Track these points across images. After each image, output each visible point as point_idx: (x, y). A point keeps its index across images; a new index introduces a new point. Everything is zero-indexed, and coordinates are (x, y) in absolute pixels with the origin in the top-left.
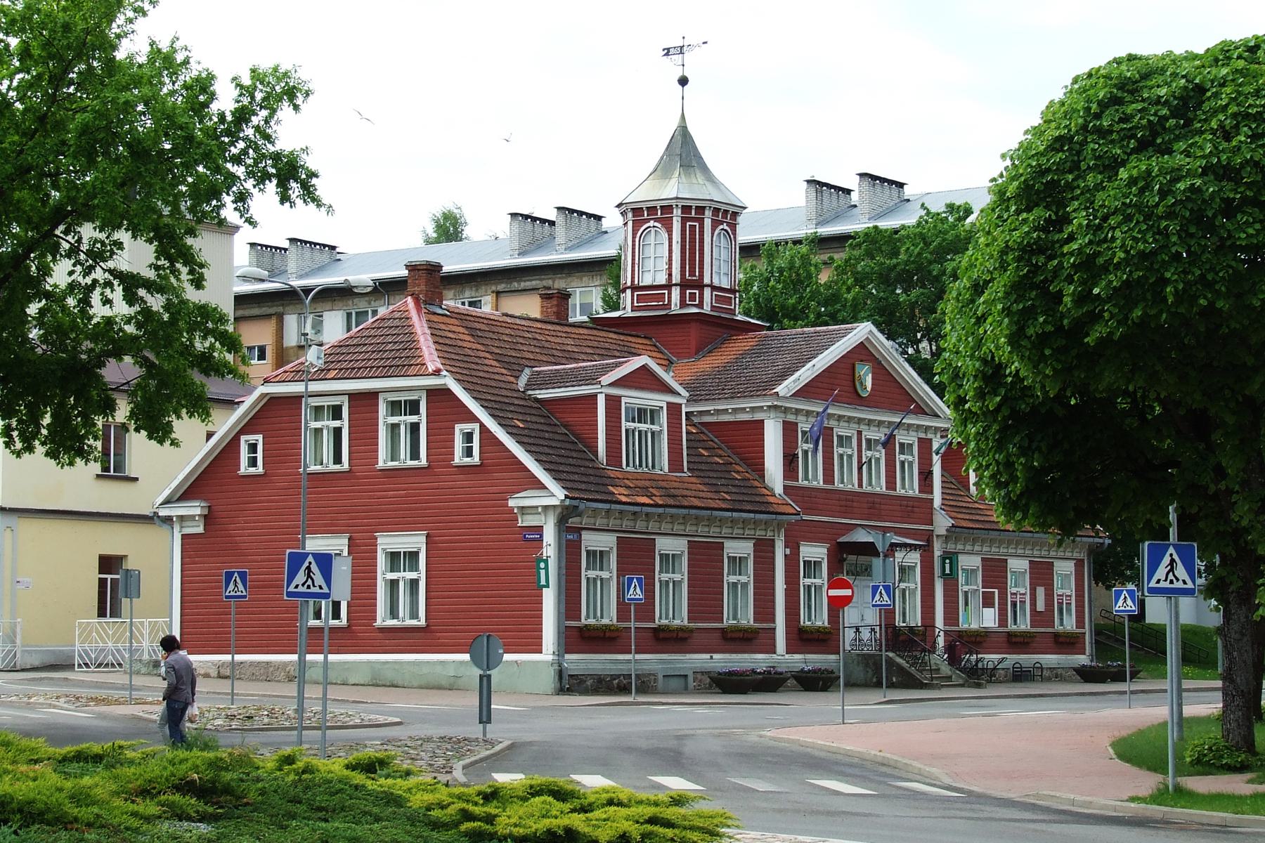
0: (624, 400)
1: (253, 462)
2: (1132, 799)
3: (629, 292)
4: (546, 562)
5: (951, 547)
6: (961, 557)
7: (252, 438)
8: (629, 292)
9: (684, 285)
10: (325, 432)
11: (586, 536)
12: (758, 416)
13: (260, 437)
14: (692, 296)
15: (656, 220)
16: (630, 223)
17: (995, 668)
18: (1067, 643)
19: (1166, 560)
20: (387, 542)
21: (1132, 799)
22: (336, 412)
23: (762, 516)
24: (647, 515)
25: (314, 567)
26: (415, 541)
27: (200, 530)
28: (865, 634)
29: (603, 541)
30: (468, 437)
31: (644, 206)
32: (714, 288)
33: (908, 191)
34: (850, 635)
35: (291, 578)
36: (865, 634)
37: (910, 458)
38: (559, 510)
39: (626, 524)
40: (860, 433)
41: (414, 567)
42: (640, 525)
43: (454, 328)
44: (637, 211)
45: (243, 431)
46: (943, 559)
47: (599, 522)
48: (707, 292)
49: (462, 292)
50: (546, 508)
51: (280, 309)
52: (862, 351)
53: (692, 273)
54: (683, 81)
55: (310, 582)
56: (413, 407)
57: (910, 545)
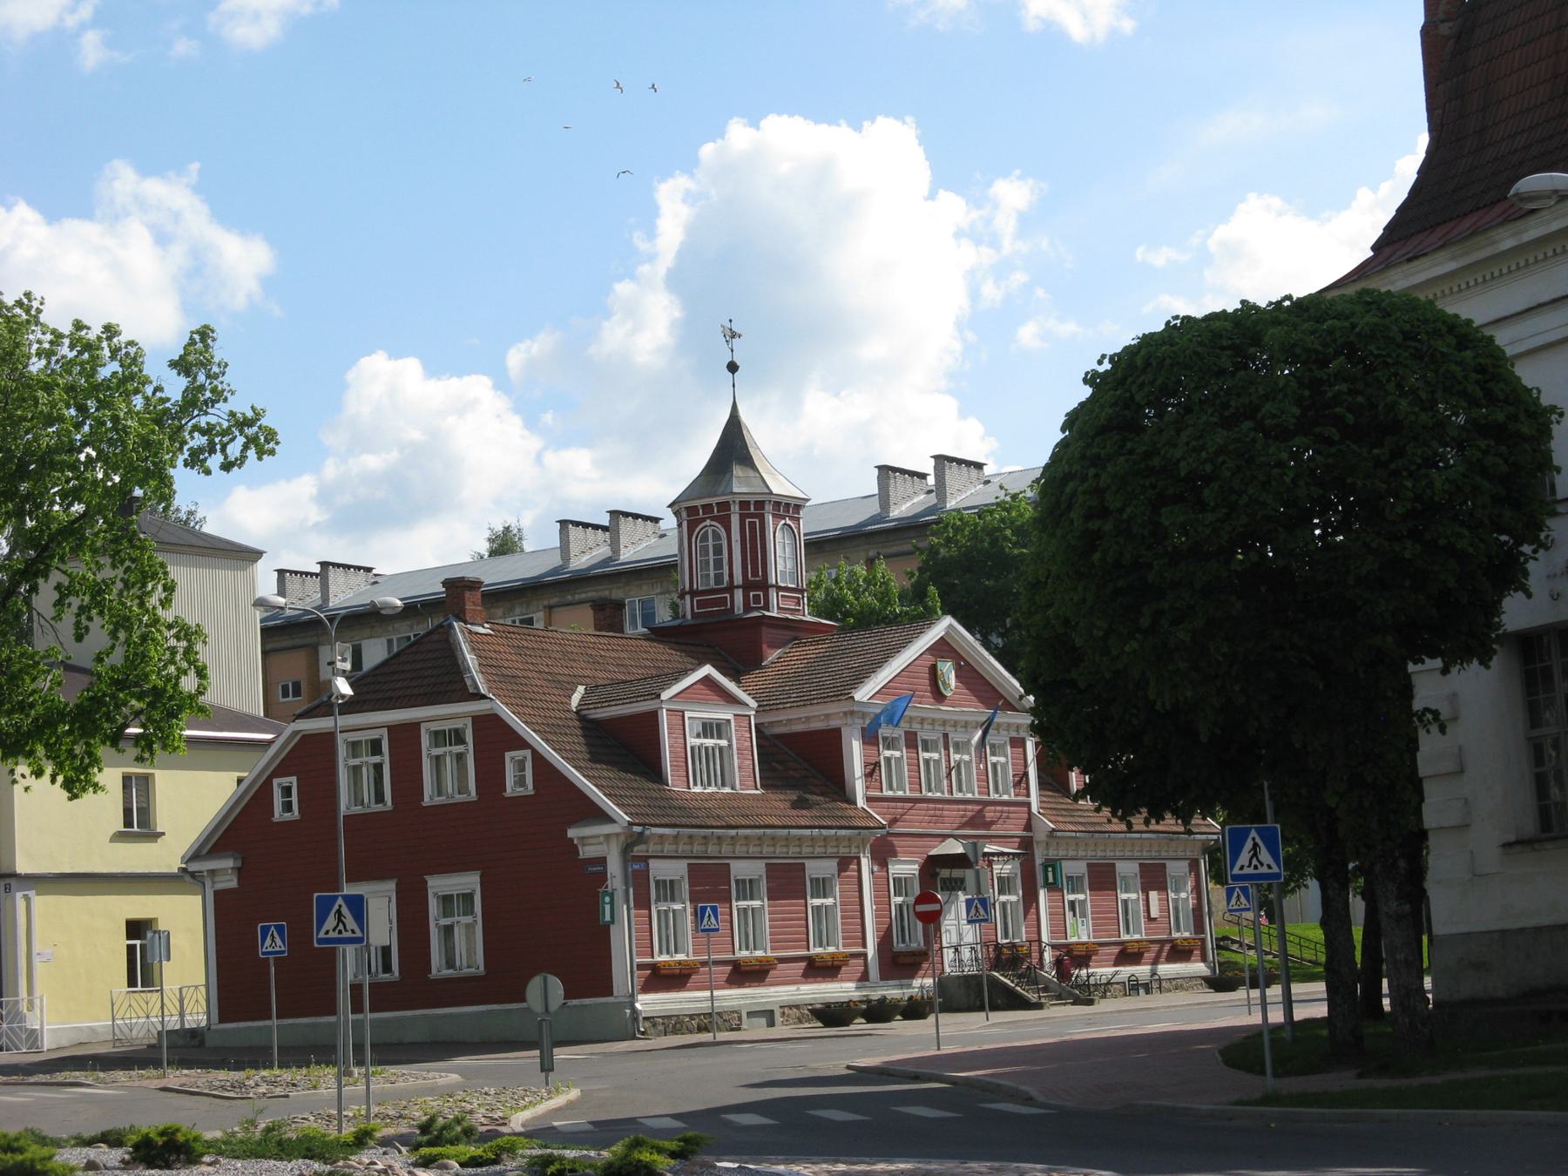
0: (687, 714)
1: (288, 807)
2: (1239, 1103)
3: (688, 597)
4: (612, 896)
5: (1052, 854)
6: (1064, 863)
7: (285, 781)
8: (688, 597)
9: (747, 586)
10: (364, 769)
11: (653, 863)
12: (834, 723)
13: (294, 779)
14: (757, 598)
15: (712, 519)
16: (685, 524)
17: (1109, 983)
18: (1179, 953)
19: (1249, 844)
20: (439, 885)
21: (1239, 1103)
22: (375, 747)
23: (843, 832)
24: (719, 838)
25: (345, 910)
26: (469, 882)
27: (234, 884)
28: (966, 954)
29: (673, 870)
30: (521, 765)
31: (698, 503)
32: (779, 588)
33: (987, 471)
34: (949, 955)
35: (321, 922)
36: (966, 954)
37: (1002, 759)
38: (622, 838)
39: (697, 848)
40: (946, 736)
41: (469, 911)
42: (712, 849)
43: (498, 648)
44: (692, 511)
45: (280, 771)
46: (1045, 868)
47: (668, 848)
48: (773, 594)
49: (511, 609)
50: (608, 837)
51: (315, 639)
52: (943, 648)
53: (755, 573)
54: (733, 367)
55: (341, 927)
56: (458, 737)
57: (1008, 854)
